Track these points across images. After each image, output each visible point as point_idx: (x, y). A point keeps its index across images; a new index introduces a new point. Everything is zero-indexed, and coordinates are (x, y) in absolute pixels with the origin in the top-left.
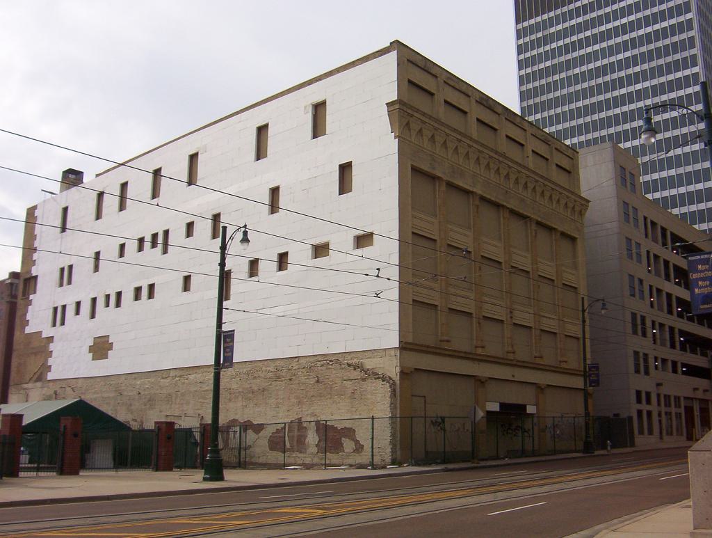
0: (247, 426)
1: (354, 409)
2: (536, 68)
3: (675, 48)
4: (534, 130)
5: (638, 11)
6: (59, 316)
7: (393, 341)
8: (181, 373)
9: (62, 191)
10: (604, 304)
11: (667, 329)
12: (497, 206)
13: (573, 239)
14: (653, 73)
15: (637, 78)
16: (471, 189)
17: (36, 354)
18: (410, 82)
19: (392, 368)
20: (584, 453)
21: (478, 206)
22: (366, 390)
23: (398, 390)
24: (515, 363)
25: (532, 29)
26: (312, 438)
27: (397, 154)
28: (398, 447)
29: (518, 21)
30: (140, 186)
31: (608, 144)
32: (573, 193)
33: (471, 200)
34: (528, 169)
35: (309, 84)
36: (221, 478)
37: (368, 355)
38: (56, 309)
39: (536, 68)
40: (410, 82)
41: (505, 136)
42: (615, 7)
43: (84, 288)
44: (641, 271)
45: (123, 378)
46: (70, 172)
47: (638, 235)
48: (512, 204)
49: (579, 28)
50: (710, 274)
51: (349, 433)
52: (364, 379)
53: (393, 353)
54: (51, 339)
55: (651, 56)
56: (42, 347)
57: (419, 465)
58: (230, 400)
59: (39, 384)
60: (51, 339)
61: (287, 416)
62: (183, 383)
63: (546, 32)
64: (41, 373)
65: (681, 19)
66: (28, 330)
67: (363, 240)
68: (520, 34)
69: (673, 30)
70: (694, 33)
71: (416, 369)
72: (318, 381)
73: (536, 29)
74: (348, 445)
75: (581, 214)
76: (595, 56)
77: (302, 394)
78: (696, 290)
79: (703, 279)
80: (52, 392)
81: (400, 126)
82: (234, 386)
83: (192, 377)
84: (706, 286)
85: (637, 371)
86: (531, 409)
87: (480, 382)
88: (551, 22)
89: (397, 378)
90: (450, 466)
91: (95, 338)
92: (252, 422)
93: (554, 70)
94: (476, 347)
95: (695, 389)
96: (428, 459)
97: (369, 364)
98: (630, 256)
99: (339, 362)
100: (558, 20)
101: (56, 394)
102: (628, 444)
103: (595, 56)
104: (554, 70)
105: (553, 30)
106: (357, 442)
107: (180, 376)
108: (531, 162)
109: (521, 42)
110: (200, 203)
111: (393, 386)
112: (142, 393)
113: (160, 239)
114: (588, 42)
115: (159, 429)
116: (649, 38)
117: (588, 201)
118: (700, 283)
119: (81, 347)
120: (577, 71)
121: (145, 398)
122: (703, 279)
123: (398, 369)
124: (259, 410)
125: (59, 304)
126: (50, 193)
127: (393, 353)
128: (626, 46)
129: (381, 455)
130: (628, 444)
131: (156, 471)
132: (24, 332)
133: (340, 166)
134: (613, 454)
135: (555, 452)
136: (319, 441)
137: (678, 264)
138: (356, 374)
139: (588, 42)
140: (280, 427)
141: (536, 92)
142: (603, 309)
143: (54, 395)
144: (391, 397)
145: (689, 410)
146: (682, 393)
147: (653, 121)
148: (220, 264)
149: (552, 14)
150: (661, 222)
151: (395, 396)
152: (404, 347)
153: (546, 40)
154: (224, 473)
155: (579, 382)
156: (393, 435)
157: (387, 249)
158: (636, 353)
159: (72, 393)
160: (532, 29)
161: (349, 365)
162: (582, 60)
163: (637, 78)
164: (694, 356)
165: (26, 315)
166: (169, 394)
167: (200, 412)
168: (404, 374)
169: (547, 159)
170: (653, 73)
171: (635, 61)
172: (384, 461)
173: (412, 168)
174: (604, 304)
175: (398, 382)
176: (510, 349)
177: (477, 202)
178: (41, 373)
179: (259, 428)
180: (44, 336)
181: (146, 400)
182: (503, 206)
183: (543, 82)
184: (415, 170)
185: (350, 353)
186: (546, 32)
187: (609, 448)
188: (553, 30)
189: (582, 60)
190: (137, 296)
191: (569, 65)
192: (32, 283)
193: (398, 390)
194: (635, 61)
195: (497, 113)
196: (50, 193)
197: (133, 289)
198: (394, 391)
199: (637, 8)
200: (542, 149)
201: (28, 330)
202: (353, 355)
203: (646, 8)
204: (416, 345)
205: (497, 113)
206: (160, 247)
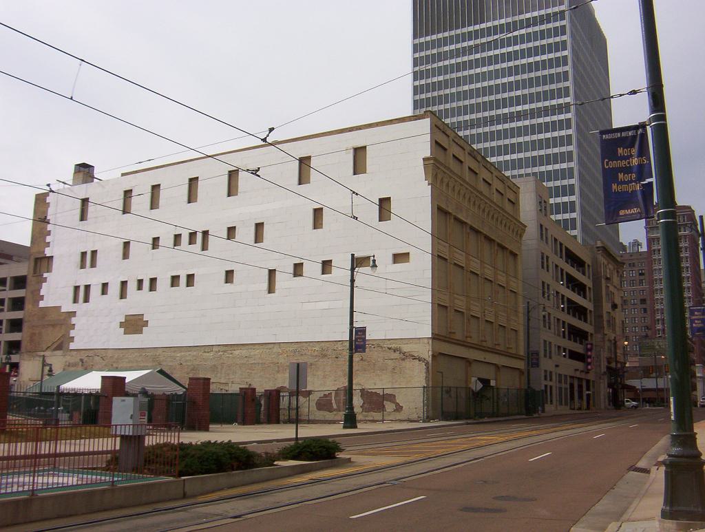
1: (394, 381)
2: (429, 81)
3: (552, 79)
4: (495, 173)
6: (82, 293)
7: (427, 332)
8: (225, 348)
9: (74, 184)
10: (544, 308)
11: (561, 322)
12: (477, 232)
13: (515, 255)
14: (532, 98)
15: (518, 101)
16: (465, 221)
17: (54, 326)
18: (436, 142)
19: (426, 352)
20: (527, 415)
21: (468, 233)
22: (405, 367)
23: (430, 368)
24: (486, 349)
25: (427, 46)
27: (430, 197)
28: (430, 408)
29: (415, 37)
30: (174, 192)
31: (531, 178)
32: (516, 219)
33: (464, 229)
34: (492, 201)
35: (350, 131)
36: (356, 427)
37: (404, 342)
38: (77, 288)
39: (429, 81)
40: (436, 142)
41: (482, 180)
43: (110, 270)
44: (548, 278)
45: (160, 351)
46: (84, 166)
47: (548, 251)
48: (485, 231)
49: (470, 50)
50: (702, 317)
51: (391, 398)
52: (403, 359)
53: (426, 341)
54: (73, 314)
55: (531, 83)
56: (62, 322)
57: (447, 420)
58: (278, 372)
59: (59, 353)
60: (73, 314)
61: (334, 385)
62: (229, 357)
63: (441, 50)
64: (62, 343)
65: (558, 54)
66: (42, 304)
67: (399, 258)
68: (416, 48)
69: (551, 64)
70: (568, 68)
72: (362, 360)
73: (432, 44)
74: (389, 407)
75: (521, 236)
76: (483, 77)
79: (698, 320)
80: (77, 360)
81: (433, 174)
82: (282, 361)
83: (237, 352)
85: (545, 356)
86: (493, 383)
87: (468, 362)
88: (445, 42)
89: (430, 360)
90: (469, 421)
91: (126, 316)
93: (446, 84)
94: (467, 337)
95: (576, 370)
96: (445, 416)
97: (406, 348)
98: (543, 267)
99: (379, 346)
100: (451, 40)
103: (483, 77)
104: (446, 84)
105: (446, 48)
106: (397, 404)
107: (224, 351)
108: (496, 197)
109: (417, 55)
110: (242, 211)
111: (427, 364)
112: (184, 364)
113: (199, 237)
114: (477, 63)
115: (245, 393)
116: (530, 68)
117: (526, 227)
119: (111, 322)
120: (466, 88)
122: (698, 320)
123: (430, 353)
125: (82, 284)
126: (63, 183)
128: (510, 71)
131: (244, 425)
132: (38, 305)
134: (543, 417)
135: (508, 415)
136: (364, 403)
137: (569, 272)
138: (397, 355)
139: (477, 63)
140: (327, 393)
141: (428, 60)
142: (543, 311)
143: (81, 363)
144: (426, 373)
145: (572, 386)
146: (571, 372)
149: (446, 34)
150: (560, 239)
151: (428, 371)
152: (436, 337)
153: (440, 57)
155: (521, 365)
157: (422, 266)
158: (545, 341)
159: (102, 361)
160: (427, 46)
161: (390, 349)
162: (471, 80)
163: (518, 101)
164: (575, 343)
165: (40, 291)
166: (215, 365)
167: (248, 380)
168: (433, 356)
169: (502, 194)
170: (532, 98)
171: (518, 85)
173: (438, 208)
174: (544, 308)
175: (431, 362)
176: (483, 339)
177: (468, 230)
178: (62, 343)
180: (63, 310)
181: (189, 370)
182: (481, 232)
183: (454, 105)
184: (440, 209)
185: (389, 340)
186: (441, 50)
187: (540, 412)
188: (446, 48)
189: (471, 80)
190: (153, 281)
191: (459, 82)
192: (45, 263)
193: (430, 368)
194: (518, 85)
195: (478, 161)
196: (63, 183)
197: (170, 277)
198: (428, 371)
200: (501, 188)
201: (42, 304)
202: (392, 341)
204: (440, 336)
205: (478, 161)
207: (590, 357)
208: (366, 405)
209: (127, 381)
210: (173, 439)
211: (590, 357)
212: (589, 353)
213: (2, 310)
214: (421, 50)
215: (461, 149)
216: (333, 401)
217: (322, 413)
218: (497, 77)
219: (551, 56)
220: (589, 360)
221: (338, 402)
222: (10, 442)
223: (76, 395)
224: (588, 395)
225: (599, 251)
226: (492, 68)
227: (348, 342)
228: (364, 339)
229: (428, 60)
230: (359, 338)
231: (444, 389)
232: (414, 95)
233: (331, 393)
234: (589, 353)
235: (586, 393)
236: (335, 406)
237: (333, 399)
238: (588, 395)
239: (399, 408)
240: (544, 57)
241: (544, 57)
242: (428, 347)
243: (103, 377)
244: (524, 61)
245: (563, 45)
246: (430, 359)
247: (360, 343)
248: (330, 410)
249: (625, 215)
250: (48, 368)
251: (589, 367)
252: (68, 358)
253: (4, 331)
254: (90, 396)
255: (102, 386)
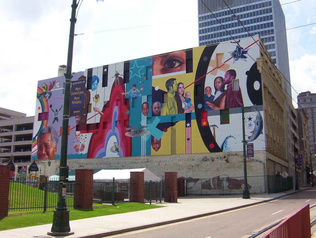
0: (190, 180)
26: (225, 184)
45: (111, 159)
65: (268, 22)
71: (269, 159)
77: (219, 167)
78: (73, 102)
84: (78, 100)
92: (192, 178)
102: (172, 201)
111: (264, 164)
118: (75, 98)
122: (77, 96)
129: (260, 190)
130: (172, 201)
136: (229, 185)
140: (208, 180)
141: (206, 24)
148: (245, 119)
154: (250, 196)
156: (265, 182)
175: (265, 163)
179: (196, 180)
206: (42, 88)
216: (212, 184)
218: (206, 32)
221: (214, 185)
222: (177, 190)
225: (301, 111)
226: (209, 27)
227: (243, 152)
228: (253, 150)
229: (206, 24)
232: (200, 40)
233: (210, 180)
236: (212, 186)
237: (211, 182)
238: (300, 180)
240: (262, 23)
241: (262, 23)
242: (264, 155)
244: (252, 25)
245: (271, 17)
247: (250, 152)
248: (210, 188)
249: (75, 113)
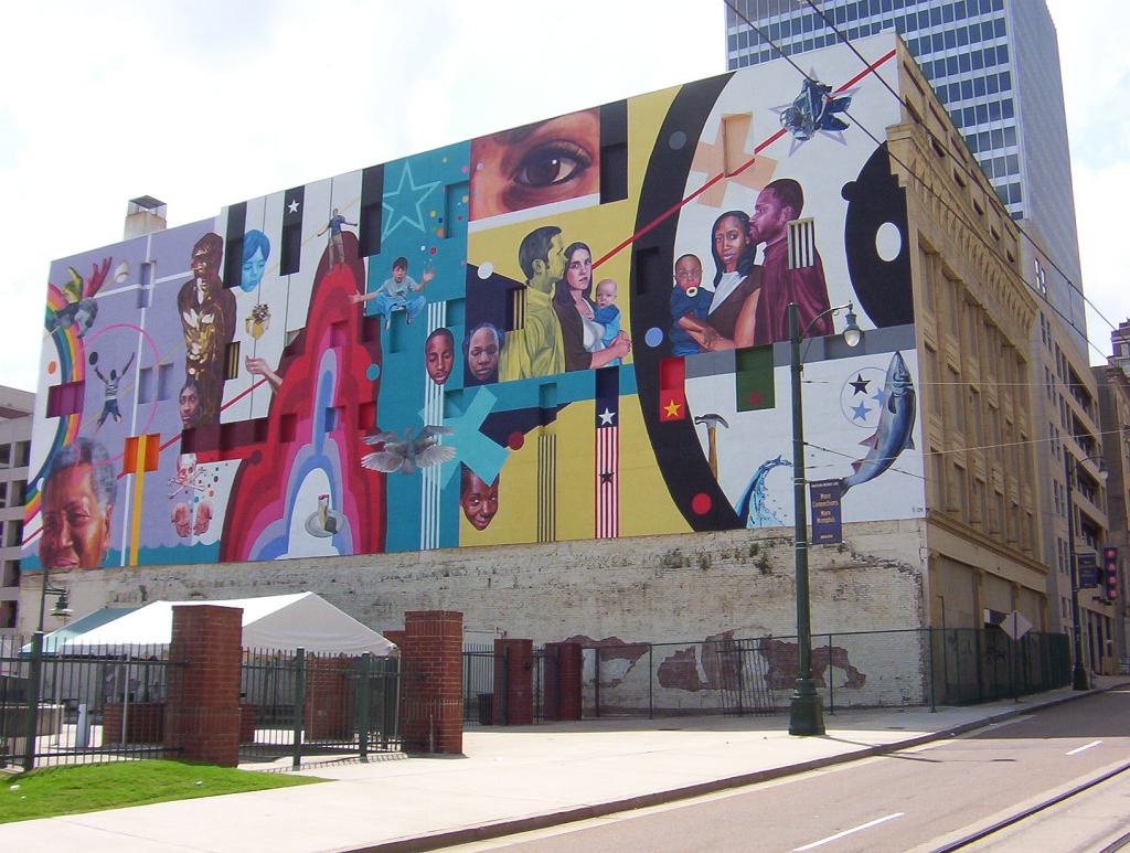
0: (610, 649)
5: (960, 16)
29: (730, 21)
42: (911, 10)
79: (825, 509)
101: (144, 593)
102: (432, 748)
106: (851, 670)
111: (919, 577)
121: (366, 600)
123: (925, 553)
124: (635, 619)
127: (913, 526)
130: (432, 748)
133: (298, 271)
140: (683, 648)
143: (140, 594)
147: (553, 294)
167: (500, 624)
172: (908, 699)
179: (636, 651)
199: (948, 13)
203: (973, 13)
207: (1113, 574)
208: (776, 674)
209: (246, 620)
210: (257, 676)
211: (1113, 574)
212: (1112, 567)
213: (1, 505)
214: (743, 46)
215: (941, 128)
216: (699, 667)
217: (673, 692)
219: (976, 47)
220: (1112, 580)
221: (709, 669)
223: (110, 660)
224: (1109, 645)
230: (825, 509)
231: (948, 632)
233: (692, 650)
234: (1112, 567)
235: (1106, 642)
236: (703, 677)
238: (1109, 645)
239: (856, 680)
240: (964, 50)
243: (174, 608)
246: (926, 566)
248: (691, 684)
250: (56, 598)
251: (1113, 593)
252: (114, 585)
253: (4, 544)
254: (148, 660)
255: (173, 639)
